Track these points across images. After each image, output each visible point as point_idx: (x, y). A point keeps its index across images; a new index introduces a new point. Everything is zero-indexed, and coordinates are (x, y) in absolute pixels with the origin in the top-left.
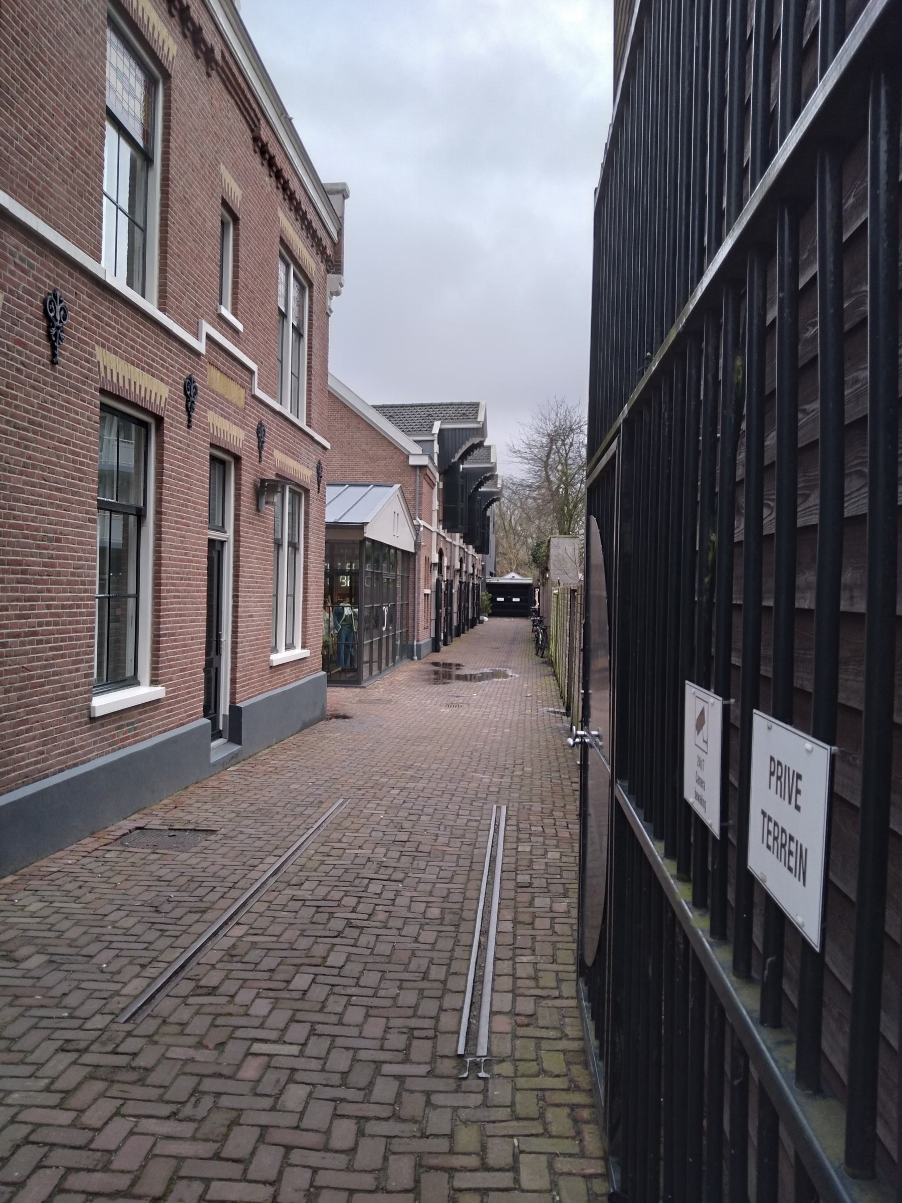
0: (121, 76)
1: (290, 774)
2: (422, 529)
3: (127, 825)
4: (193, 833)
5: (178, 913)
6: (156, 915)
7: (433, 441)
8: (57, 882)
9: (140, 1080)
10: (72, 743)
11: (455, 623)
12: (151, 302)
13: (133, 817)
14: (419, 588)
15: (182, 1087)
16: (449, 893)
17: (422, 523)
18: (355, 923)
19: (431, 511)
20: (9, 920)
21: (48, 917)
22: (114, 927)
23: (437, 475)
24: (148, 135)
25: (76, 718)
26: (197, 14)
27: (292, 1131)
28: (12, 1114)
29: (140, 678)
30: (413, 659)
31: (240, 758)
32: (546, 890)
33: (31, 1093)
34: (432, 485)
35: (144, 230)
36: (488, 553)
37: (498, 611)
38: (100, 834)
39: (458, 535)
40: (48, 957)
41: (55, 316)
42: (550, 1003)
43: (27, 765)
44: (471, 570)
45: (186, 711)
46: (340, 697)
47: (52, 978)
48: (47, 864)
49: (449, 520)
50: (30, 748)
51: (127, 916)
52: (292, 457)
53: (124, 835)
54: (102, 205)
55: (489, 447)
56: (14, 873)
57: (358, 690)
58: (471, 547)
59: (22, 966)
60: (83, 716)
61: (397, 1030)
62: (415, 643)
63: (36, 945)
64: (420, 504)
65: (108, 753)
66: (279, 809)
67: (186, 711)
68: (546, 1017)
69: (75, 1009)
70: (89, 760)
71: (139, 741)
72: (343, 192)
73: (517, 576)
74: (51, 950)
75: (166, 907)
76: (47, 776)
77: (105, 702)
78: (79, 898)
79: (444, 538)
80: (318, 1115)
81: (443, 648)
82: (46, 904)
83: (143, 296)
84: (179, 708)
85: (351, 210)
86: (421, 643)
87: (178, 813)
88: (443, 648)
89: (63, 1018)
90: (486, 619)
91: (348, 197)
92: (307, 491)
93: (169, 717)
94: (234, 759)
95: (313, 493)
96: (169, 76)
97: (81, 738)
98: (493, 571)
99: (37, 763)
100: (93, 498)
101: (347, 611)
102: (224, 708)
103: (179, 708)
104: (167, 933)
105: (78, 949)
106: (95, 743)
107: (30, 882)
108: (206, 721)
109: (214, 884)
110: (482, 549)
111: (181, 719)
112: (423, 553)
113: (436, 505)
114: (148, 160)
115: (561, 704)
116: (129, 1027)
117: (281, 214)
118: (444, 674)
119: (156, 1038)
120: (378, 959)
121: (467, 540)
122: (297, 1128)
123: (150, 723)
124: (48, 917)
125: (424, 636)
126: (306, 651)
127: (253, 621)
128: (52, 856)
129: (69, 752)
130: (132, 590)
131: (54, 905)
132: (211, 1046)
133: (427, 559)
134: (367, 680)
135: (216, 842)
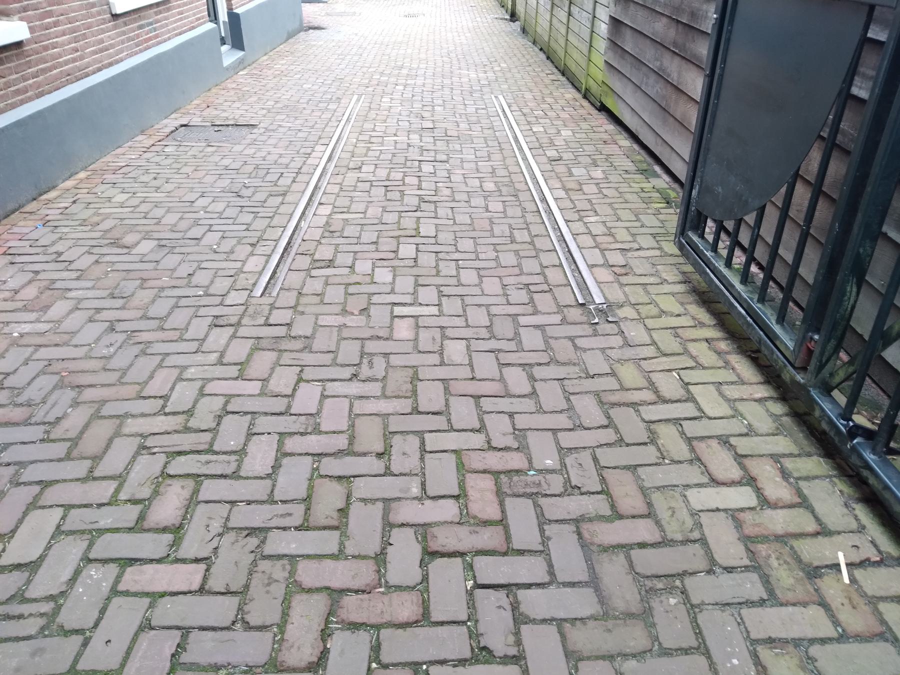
1: (299, 76)
3: (172, 122)
4: (236, 128)
5: (260, 196)
6: (239, 199)
8: (130, 175)
9: (305, 348)
10: (102, 41)
13: (173, 116)
15: (350, 352)
16: (494, 169)
18: (427, 198)
20: (101, 211)
21: (138, 206)
22: (206, 212)
25: (99, 14)
27: (470, 382)
28: (198, 387)
31: (246, 63)
32: (576, 161)
33: (206, 367)
38: (150, 132)
40: (156, 242)
42: (636, 254)
43: (66, 63)
45: (194, 14)
47: (171, 261)
48: (110, 159)
50: (63, 45)
51: (213, 201)
53: (172, 132)
56: (84, 169)
59: (134, 251)
60: (104, 12)
61: (513, 287)
63: (140, 232)
65: (136, 53)
66: (305, 105)
67: (194, 14)
68: (640, 267)
69: (208, 287)
70: (122, 60)
74: (156, 235)
75: (245, 192)
76: (87, 75)
78: (159, 188)
80: (486, 366)
82: (130, 195)
84: (188, 10)
87: (211, 112)
89: (200, 296)
93: (181, 19)
94: (240, 65)
97: (109, 37)
99: (74, 60)
102: (223, 16)
103: (188, 10)
104: (259, 215)
105: (182, 234)
106: (123, 42)
107: (104, 177)
108: (212, 25)
109: (282, 171)
111: (192, 23)
115: (504, 12)
116: (267, 300)
119: (300, 308)
122: (473, 379)
123: (167, 25)
124: (138, 206)
128: (113, 153)
129: (101, 51)
131: (138, 195)
132: (356, 313)
135: (261, 134)
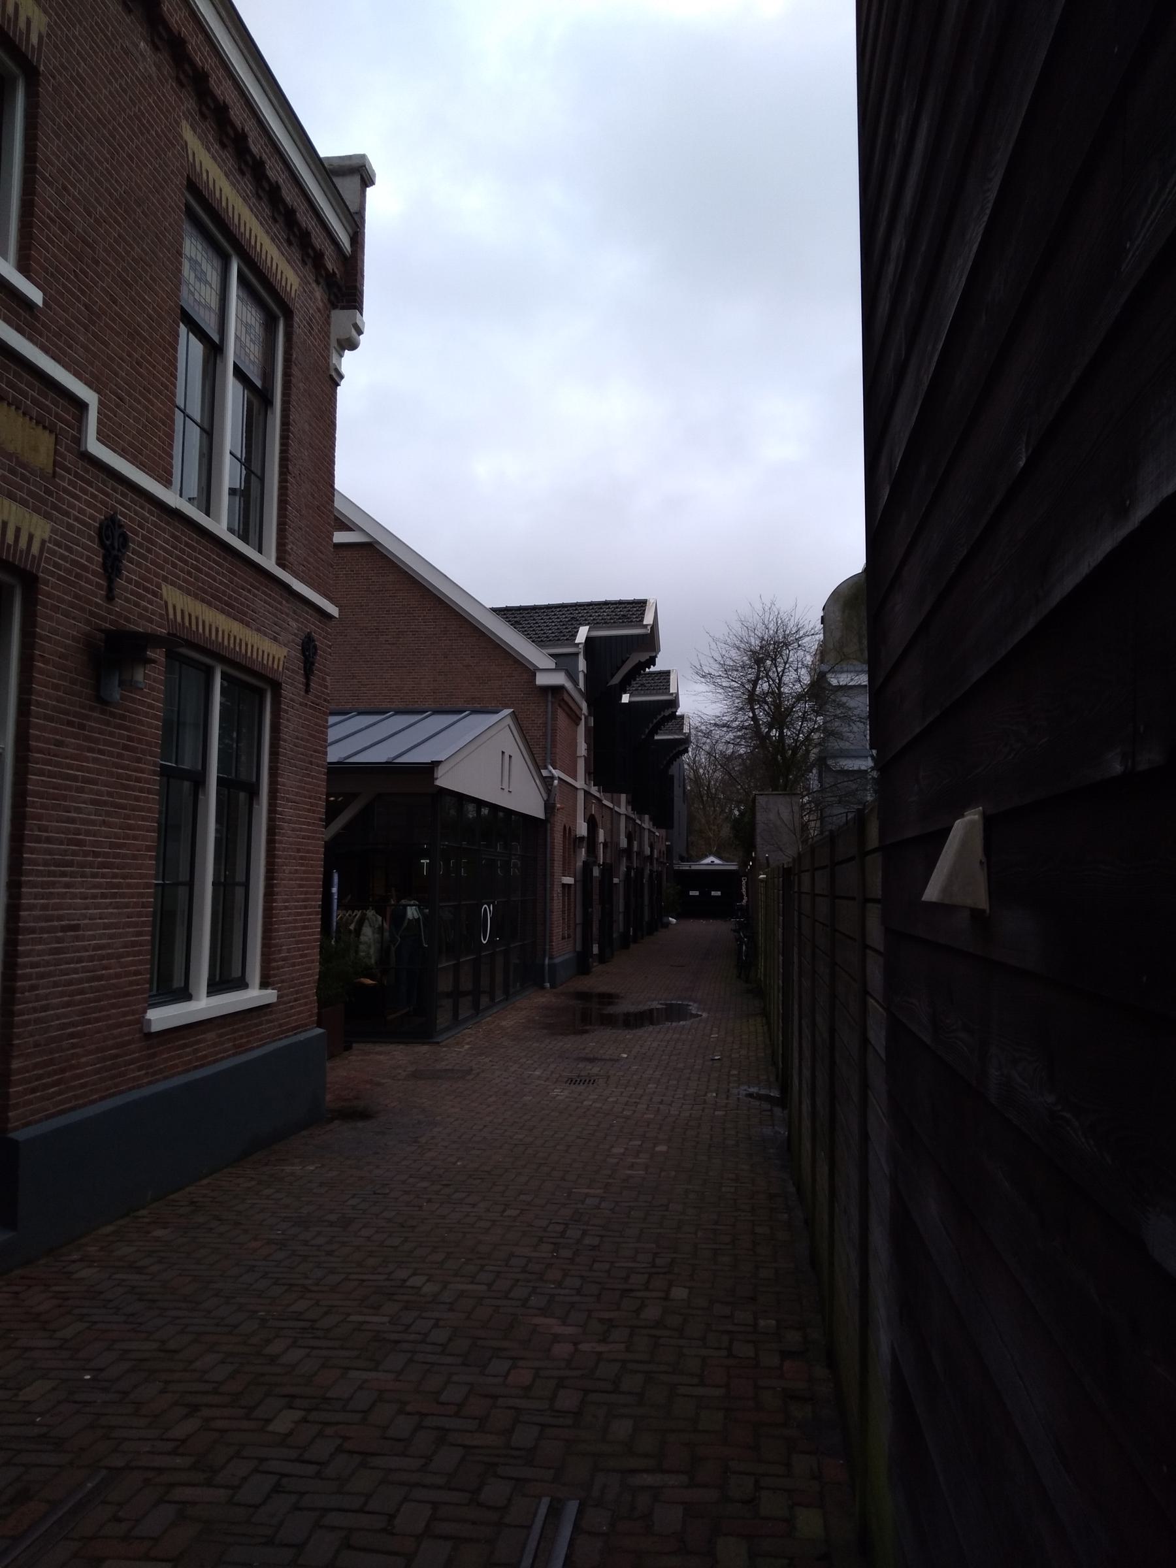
0: (194, 263)
2: (556, 782)
7: (577, 654)
11: (646, 918)
12: (269, 558)
14: (552, 875)
17: (556, 773)
19: (574, 758)
23: (584, 705)
24: (268, 374)
26: (175, 17)
29: (248, 979)
30: (543, 988)
34: (575, 719)
35: (262, 479)
36: (672, 827)
37: (689, 910)
39: (623, 797)
41: (112, 544)
44: (647, 851)
46: (382, 1064)
49: (602, 771)
52: (223, 611)
54: (173, 421)
55: (682, 717)
57: (425, 1048)
58: (647, 817)
62: (547, 961)
64: (554, 745)
71: (85, 1105)
72: (359, 172)
73: (717, 861)
77: (162, 1017)
79: (599, 800)
81: (597, 968)
83: (260, 551)
85: (378, 205)
86: (557, 961)
88: (597, 968)
90: (673, 920)
91: (372, 183)
92: (276, 686)
95: (291, 691)
96: (292, 312)
98: (685, 854)
100: (155, 764)
101: (412, 912)
110: (664, 819)
112: (559, 821)
113: (582, 749)
114: (268, 402)
117: (188, 135)
118: (592, 1013)
120: (567, 1291)
121: (637, 805)
125: (561, 948)
126: (269, 991)
127: (77, 938)
130: (240, 877)
133: (568, 832)
134: (448, 1029)
